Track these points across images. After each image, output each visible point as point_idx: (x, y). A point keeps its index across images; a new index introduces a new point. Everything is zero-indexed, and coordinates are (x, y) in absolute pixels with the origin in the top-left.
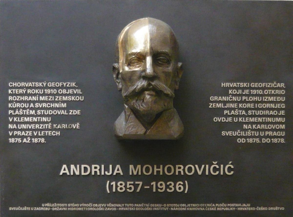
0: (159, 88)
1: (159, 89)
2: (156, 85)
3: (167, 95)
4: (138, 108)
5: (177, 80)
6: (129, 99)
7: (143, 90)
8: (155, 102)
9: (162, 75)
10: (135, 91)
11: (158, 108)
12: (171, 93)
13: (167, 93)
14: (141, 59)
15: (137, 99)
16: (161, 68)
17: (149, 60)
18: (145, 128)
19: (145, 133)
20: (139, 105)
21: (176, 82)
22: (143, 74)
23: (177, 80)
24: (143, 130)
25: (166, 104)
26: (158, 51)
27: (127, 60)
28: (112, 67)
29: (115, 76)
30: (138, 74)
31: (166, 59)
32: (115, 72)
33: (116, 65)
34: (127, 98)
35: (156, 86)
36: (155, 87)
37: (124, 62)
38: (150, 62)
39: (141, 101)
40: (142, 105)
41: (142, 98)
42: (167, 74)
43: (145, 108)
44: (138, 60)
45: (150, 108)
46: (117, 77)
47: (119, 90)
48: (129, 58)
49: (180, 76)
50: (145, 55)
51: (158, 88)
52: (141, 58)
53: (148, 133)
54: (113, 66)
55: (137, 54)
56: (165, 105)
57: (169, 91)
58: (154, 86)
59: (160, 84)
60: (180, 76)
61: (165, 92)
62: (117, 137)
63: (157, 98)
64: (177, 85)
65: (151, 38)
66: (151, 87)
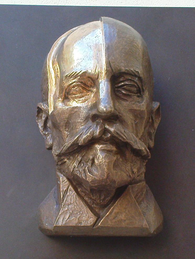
0: (124, 137)
1: (124, 139)
2: (119, 132)
3: (137, 153)
4: (83, 176)
5: (152, 131)
6: (66, 160)
7: (92, 141)
8: (116, 165)
9: (129, 118)
10: (78, 144)
11: (121, 176)
12: (145, 149)
13: (138, 148)
14: (88, 86)
15: (81, 160)
16: (124, 103)
17: (104, 86)
18: (96, 214)
19: (95, 224)
20: (84, 170)
21: (150, 134)
22: (94, 112)
23: (152, 131)
24: (91, 219)
25: (135, 170)
26: (120, 70)
27: (61, 88)
28: (47, 150)
29: (40, 125)
30: (84, 113)
31: (136, 87)
32: (41, 117)
33: (43, 106)
34: (62, 158)
35: (117, 133)
36: (117, 136)
37: (58, 94)
38: (107, 90)
39: (89, 164)
40: (90, 172)
41: (91, 157)
42: (137, 115)
43: (96, 176)
44: (83, 88)
45: (106, 175)
46: (45, 127)
47: (48, 147)
48: (66, 85)
49: (156, 125)
50: (97, 77)
51: (122, 137)
52: (87, 82)
53: (100, 224)
54: (38, 108)
55: (81, 76)
56: (133, 172)
57: (141, 146)
58: (115, 135)
59: (125, 131)
60: (156, 125)
61: (135, 147)
62: (43, 230)
63: (119, 157)
64: (151, 139)
65: (109, 46)
66: (109, 135)
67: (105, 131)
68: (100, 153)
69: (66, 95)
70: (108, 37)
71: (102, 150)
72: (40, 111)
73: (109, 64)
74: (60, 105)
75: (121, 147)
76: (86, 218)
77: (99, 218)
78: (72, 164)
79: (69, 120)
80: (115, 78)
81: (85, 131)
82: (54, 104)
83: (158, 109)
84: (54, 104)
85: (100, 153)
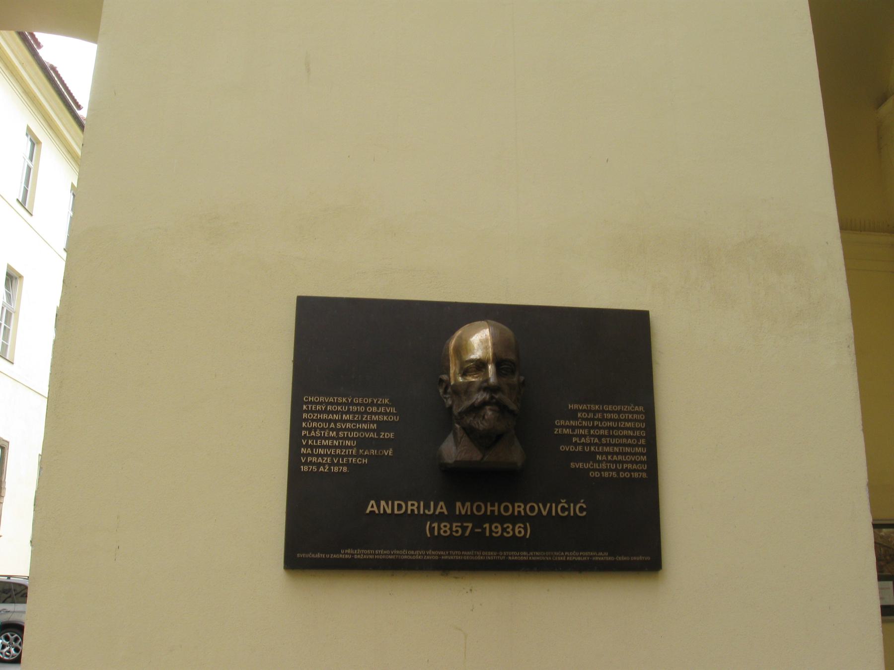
3: (512, 412)
7: (484, 404)
17: (491, 368)
19: (482, 459)
22: (485, 384)
29: (441, 391)
33: (445, 377)
46: (445, 392)
48: (466, 366)
52: (480, 365)
57: (513, 407)
67: (492, 398)
68: (489, 413)
69: (465, 373)
70: (493, 335)
71: (491, 410)
72: (441, 381)
73: (494, 354)
74: (460, 379)
75: (502, 408)
76: (475, 455)
77: (484, 456)
78: (469, 420)
79: (467, 388)
80: (499, 363)
81: (479, 397)
82: (455, 377)
83: (524, 381)
84: (455, 377)
85: (489, 413)
